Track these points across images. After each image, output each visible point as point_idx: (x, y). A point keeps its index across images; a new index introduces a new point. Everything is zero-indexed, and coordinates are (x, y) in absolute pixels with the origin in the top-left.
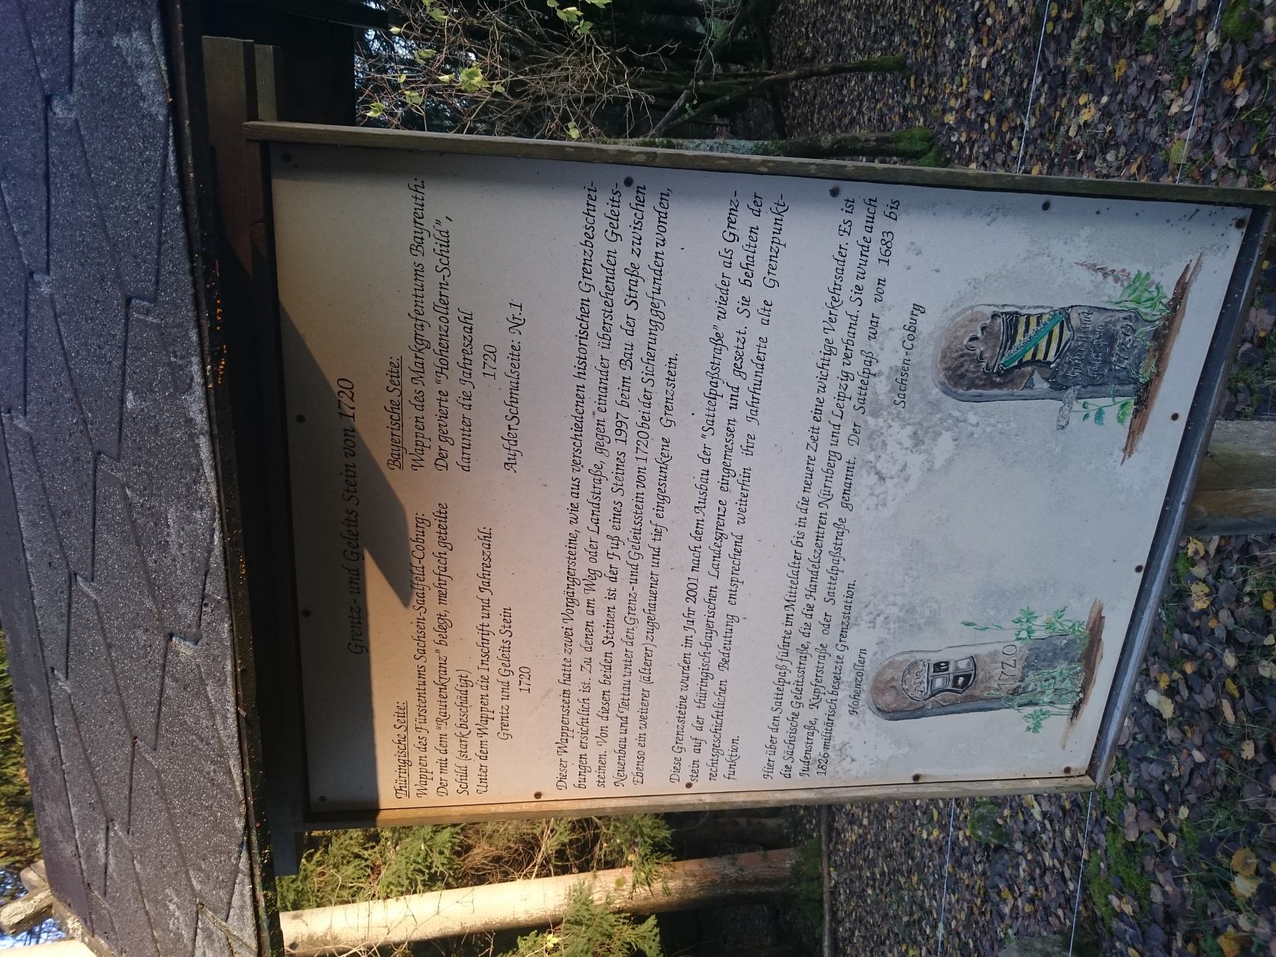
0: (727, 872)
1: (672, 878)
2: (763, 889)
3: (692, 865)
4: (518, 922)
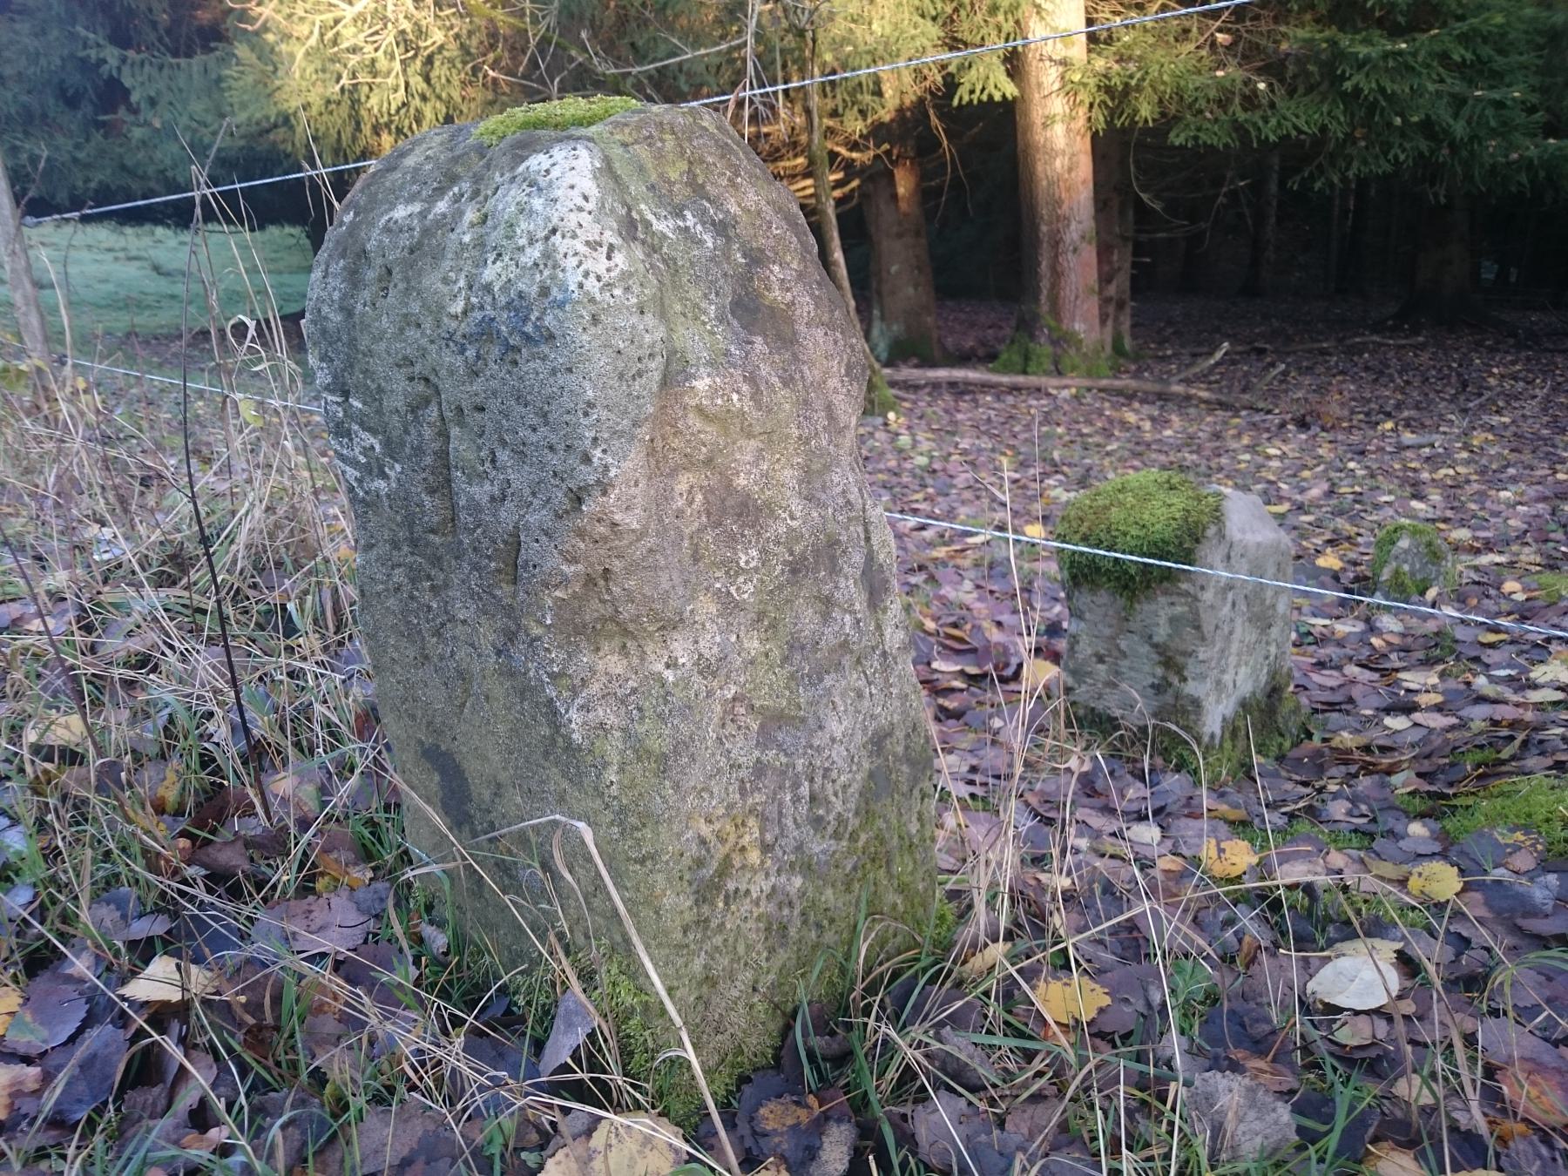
1: (1068, 130)
2: (1045, 285)
3: (1085, 168)
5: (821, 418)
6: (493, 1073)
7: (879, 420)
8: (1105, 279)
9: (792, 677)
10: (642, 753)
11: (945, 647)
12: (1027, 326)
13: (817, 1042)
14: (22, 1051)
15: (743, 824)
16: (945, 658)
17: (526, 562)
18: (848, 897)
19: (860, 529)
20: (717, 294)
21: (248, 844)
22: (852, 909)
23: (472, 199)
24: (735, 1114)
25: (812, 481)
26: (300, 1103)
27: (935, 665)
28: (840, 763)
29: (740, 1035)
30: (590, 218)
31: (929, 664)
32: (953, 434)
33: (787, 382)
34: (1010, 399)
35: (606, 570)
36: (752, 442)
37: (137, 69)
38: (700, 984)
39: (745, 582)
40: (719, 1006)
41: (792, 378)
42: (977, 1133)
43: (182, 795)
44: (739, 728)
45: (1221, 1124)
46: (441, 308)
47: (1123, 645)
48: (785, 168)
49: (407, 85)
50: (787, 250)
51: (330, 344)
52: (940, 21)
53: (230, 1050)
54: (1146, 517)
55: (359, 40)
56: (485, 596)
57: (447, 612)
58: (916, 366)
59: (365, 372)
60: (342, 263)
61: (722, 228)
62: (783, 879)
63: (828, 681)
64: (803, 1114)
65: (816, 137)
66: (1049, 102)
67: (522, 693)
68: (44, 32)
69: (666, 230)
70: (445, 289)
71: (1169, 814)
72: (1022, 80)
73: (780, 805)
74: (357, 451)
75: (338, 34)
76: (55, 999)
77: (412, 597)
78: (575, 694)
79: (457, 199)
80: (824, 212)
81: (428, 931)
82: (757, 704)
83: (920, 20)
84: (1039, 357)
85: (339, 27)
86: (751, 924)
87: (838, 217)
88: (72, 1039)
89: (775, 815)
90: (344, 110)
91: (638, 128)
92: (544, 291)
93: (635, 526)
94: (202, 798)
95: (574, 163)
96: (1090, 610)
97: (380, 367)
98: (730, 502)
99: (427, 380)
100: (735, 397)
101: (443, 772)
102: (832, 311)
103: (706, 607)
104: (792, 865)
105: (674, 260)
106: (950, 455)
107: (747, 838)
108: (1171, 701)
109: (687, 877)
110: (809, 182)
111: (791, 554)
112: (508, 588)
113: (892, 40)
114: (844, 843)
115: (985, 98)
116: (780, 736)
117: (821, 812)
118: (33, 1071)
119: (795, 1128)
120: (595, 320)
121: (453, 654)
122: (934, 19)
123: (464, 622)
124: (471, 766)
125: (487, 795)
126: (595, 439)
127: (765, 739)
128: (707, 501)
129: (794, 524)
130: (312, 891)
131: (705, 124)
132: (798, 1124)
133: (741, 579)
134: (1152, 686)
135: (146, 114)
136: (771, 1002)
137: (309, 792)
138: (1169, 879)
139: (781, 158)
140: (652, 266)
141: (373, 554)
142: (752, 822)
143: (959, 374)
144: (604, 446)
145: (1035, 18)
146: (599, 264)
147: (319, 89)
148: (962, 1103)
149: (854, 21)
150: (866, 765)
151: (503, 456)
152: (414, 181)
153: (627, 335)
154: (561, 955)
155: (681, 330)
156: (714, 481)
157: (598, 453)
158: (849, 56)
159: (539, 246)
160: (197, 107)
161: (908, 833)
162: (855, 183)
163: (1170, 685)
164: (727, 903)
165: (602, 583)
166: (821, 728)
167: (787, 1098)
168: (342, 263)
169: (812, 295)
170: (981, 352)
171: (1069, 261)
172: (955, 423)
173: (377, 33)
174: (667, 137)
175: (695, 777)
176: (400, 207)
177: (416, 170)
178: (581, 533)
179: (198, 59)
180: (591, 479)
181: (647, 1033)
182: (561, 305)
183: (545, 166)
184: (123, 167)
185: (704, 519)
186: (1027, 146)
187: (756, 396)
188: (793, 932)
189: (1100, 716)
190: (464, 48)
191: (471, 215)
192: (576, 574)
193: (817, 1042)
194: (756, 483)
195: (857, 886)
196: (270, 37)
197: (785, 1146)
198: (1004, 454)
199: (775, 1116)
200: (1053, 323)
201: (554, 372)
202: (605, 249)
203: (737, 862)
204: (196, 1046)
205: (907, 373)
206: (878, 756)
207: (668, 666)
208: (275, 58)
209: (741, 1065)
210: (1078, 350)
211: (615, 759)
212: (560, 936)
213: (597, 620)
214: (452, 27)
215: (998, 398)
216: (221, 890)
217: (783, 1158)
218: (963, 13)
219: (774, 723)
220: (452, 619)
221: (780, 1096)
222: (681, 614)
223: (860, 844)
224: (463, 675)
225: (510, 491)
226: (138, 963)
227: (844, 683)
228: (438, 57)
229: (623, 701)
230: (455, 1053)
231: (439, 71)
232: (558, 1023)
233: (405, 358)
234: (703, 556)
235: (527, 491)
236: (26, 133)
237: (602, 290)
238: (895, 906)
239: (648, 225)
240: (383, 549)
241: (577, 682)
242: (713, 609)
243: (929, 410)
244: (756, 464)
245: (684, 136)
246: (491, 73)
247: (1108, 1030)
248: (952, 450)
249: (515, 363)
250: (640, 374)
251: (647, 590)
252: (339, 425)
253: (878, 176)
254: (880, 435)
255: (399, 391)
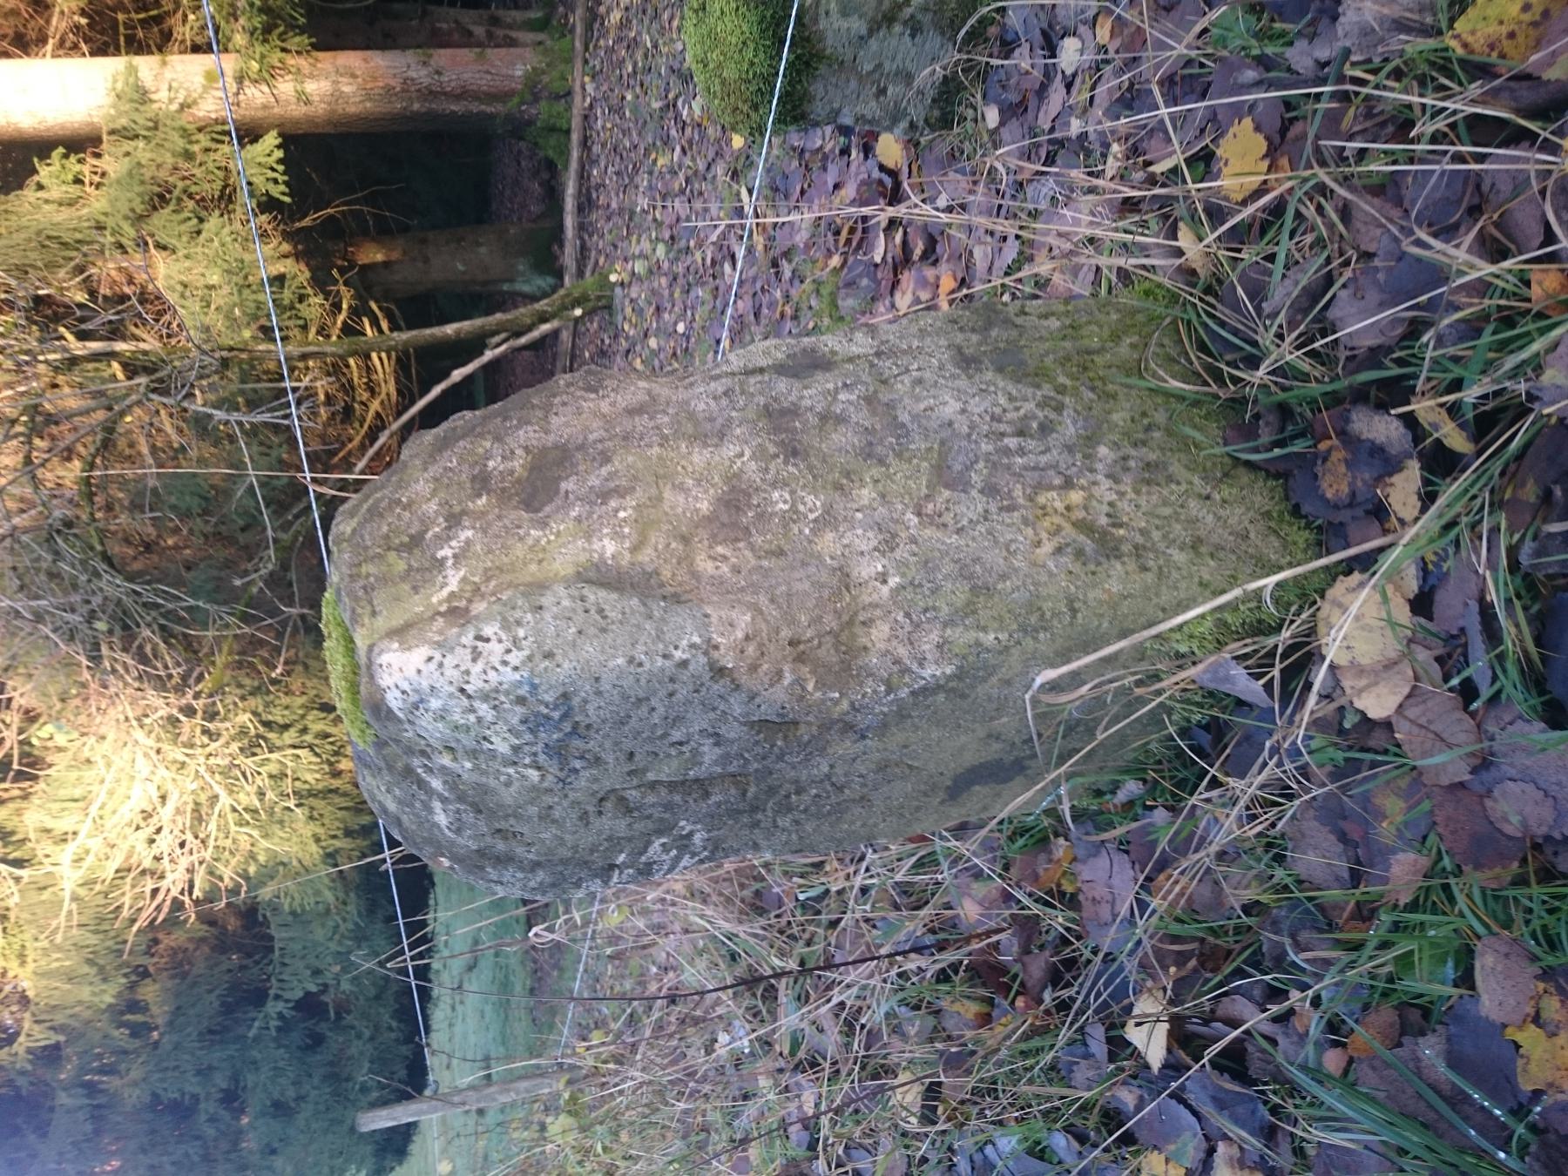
0: (413, 74)
1: (311, 76)
2: (475, 107)
3: (351, 59)
4: (19, 130)
5: (642, 422)
6: (1266, 753)
7: (618, 290)
8: (466, 39)
9: (899, 455)
10: (969, 610)
11: (859, 246)
12: (518, 127)
13: (1265, 437)
14: (1202, 1155)
15: (1043, 508)
16: (871, 248)
17: (778, 715)
18: (1121, 396)
19: (752, 380)
20: (519, 527)
21: (1026, 951)
22: (1133, 392)
23: (429, 758)
24: (1330, 523)
25: (711, 433)
26: (1275, 926)
27: (878, 259)
28: (986, 404)
29: (1251, 513)
30: (449, 657)
31: (876, 265)
32: (632, 213)
33: (606, 458)
34: (596, 149)
35: (791, 644)
36: (666, 495)
37: (285, 986)
38: (1198, 554)
39: (804, 504)
40: (1222, 536)
41: (602, 453)
42: (1376, 282)
43: (975, 999)
44: (947, 509)
45: (1394, 21)
46: (534, 788)
47: (868, 67)
48: (360, 377)
49: (295, 747)
50: (472, 452)
51: (565, 880)
52: (204, 214)
53: (1220, 985)
54: (734, 41)
55: (252, 789)
56: (809, 750)
57: (822, 781)
58: (562, 246)
59: (592, 851)
60: (489, 870)
61: (454, 521)
62: (1099, 466)
63: (904, 417)
64: (1337, 456)
65: (329, 349)
66: (283, 97)
67: (903, 717)
68: (255, 1062)
69: (458, 578)
70: (516, 785)
71: (1050, 26)
72: (261, 126)
73: (1025, 468)
74: (665, 857)
75: (245, 809)
76: (1156, 1125)
77: (805, 811)
78: (908, 670)
79: (430, 770)
80: (406, 343)
81: (1121, 796)
82: (924, 491)
83: (204, 235)
84: (550, 116)
85: (239, 808)
86: (1143, 501)
87: (410, 327)
88: (1195, 1113)
89: (1036, 474)
90: (318, 804)
91: (356, 599)
92: (521, 701)
93: (748, 618)
94: (978, 981)
95: (395, 667)
96: (830, 102)
97: (587, 839)
98: (725, 518)
99: (602, 800)
100: (622, 514)
101: (972, 783)
102: (533, 407)
103: (828, 543)
104: (1086, 456)
105: (486, 570)
106: (655, 220)
107: (1059, 505)
108: (929, 16)
109: (1092, 567)
110: (374, 355)
111: (777, 456)
112: (803, 729)
113: (226, 266)
114: (1067, 400)
115: (281, 168)
116: (958, 467)
117: (1035, 425)
118: (1222, 1147)
119: (1349, 464)
120: (549, 655)
121: (861, 776)
122: (201, 220)
123: (832, 767)
124: (970, 758)
125: (996, 746)
126: (665, 656)
127: (959, 484)
128: (724, 542)
129: (748, 453)
130: (1074, 896)
131: (349, 530)
132: (1346, 461)
133: (801, 508)
134: (913, 36)
135: (328, 978)
136: (1221, 481)
137: (979, 889)
138: (1122, 33)
139: (350, 381)
140: (493, 594)
141: (763, 843)
142: (1041, 499)
143: (570, 204)
144: (671, 648)
145: (194, 110)
146: (494, 650)
147: (299, 825)
148: (1344, 294)
149: (208, 306)
150: (989, 375)
151: (677, 735)
152: (411, 805)
153: (562, 624)
154: (1158, 686)
155: (557, 566)
156: (704, 534)
157: (678, 655)
158: (244, 313)
159: (477, 704)
160: (319, 934)
161: (1060, 330)
162: (374, 306)
163: (912, 16)
164: (1121, 525)
165: (802, 647)
166: (950, 424)
167: (1319, 469)
168: (489, 870)
169: (518, 427)
170: (545, 175)
171: (450, 80)
172: (621, 211)
173: (244, 774)
174: (364, 569)
175: (995, 558)
176: (436, 818)
177: (400, 802)
178: (754, 668)
179: (273, 931)
180: (703, 660)
181: (1242, 608)
182: (534, 687)
183: (398, 694)
184: (377, 997)
185: (741, 545)
186: (329, 122)
187: (620, 492)
188: (1152, 457)
189: (941, 93)
190: (254, 692)
191: (446, 760)
192: (793, 671)
193: (1265, 437)
194: (706, 492)
195: (1110, 387)
196: (252, 869)
197: (1367, 476)
198: (655, 161)
199: (1336, 483)
200: (516, 100)
201: (599, 693)
202: (480, 644)
203: (1079, 514)
204: (1213, 1011)
205: (569, 258)
206: (981, 362)
207: (885, 582)
208: (271, 864)
209: (1281, 513)
210: (544, 72)
211: (972, 635)
212: (1139, 683)
213: (837, 651)
214: (235, 704)
215: (595, 162)
216: (1068, 976)
217: (1379, 479)
218: (193, 189)
219: (946, 476)
220: (828, 777)
221: (1316, 477)
222: (834, 569)
223: (1068, 382)
224: (882, 767)
225: (710, 730)
226: (1129, 1051)
227: (907, 401)
228: (265, 717)
229: (917, 626)
230: (1247, 787)
231: (277, 716)
232: (1225, 688)
233: (581, 819)
234: (779, 546)
235: (712, 715)
236: (347, 1080)
237: (520, 649)
238: (1133, 346)
239: (452, 594)
240: (758, 835)
241: (896, 668)
242: (830, 536)
243: (608, 237)
244: (686, 491)
245: (363, 554)
246: (279, 671)
247: (1278, 124)
248: (650, 217)
249: (588, 727)
250: (601, 611)
251: (810, 604)
252: (640, 872)
253: (367, 282)
254: (634, 292)
255: (611, 823)
